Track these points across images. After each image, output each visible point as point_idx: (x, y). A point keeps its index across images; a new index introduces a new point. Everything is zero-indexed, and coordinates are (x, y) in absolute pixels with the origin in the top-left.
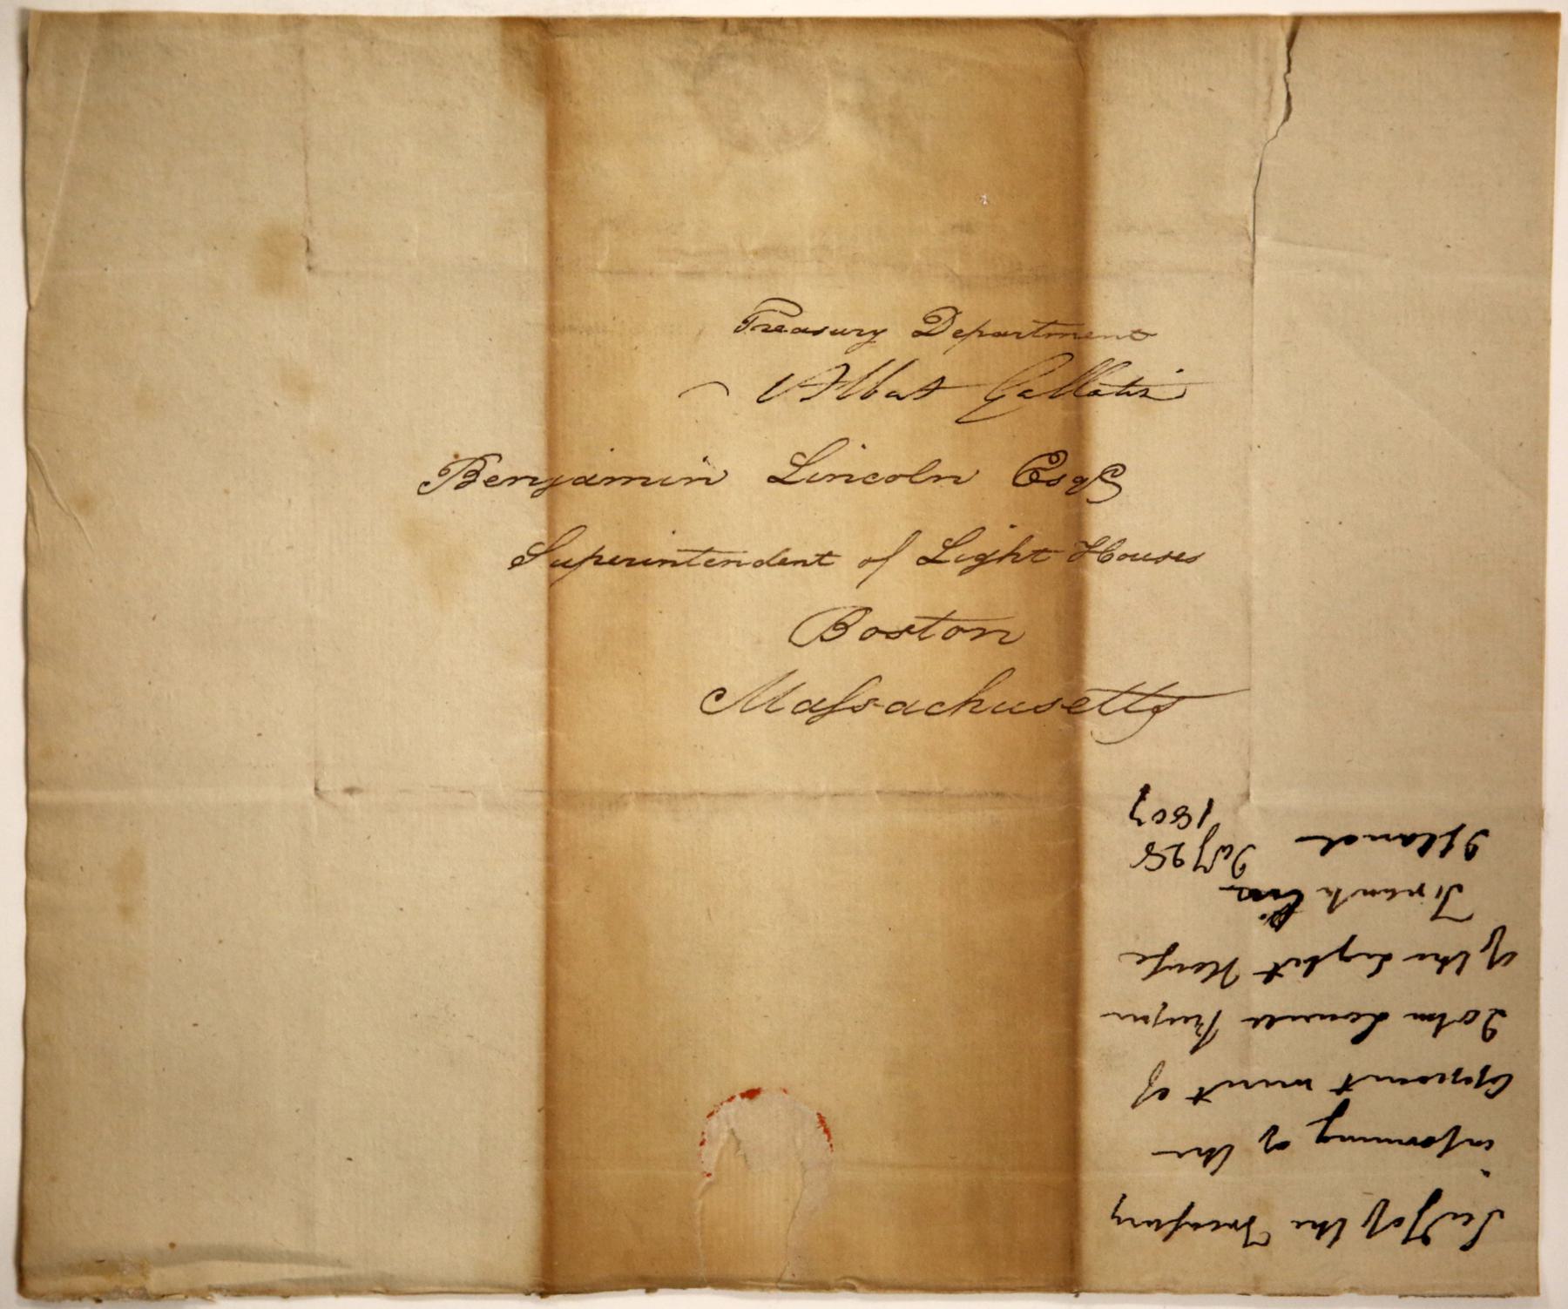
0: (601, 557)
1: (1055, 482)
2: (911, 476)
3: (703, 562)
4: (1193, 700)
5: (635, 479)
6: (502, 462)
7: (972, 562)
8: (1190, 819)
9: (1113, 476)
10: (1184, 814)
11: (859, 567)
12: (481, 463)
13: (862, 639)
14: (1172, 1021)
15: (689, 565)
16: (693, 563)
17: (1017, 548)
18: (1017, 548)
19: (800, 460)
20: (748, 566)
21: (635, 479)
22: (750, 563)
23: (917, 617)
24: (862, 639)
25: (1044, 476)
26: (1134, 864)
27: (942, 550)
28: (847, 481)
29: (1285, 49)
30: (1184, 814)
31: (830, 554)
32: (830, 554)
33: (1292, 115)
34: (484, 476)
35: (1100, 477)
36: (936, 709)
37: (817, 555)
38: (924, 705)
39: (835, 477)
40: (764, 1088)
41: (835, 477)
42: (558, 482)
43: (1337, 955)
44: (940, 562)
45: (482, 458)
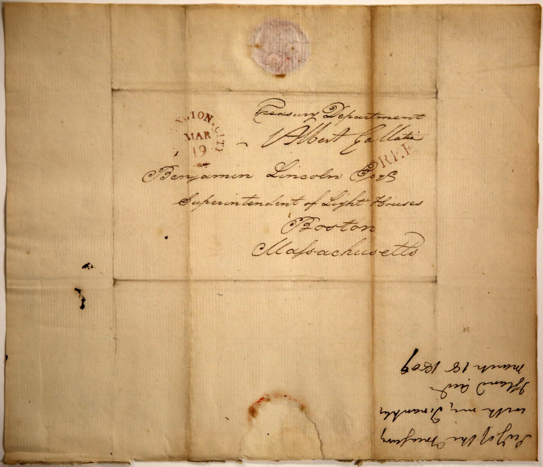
1: (310, 252)
2: (321, 176)
4: (284, 239)
8: (459, 369)
9: (393, 174)
10: (457, 367)
12: (171, 169)
13: (388, 251)
14: (415, 440)
20: (199, 179)
23: (368, 114)
24: (388, 251)
28: (295, 178)
29: (386, 137)
30: (457, 367)
34: (172, 175)
35: (388, 175)
38: (301, 176)
39: (290, 176)
40: (254, 420)
41: (290, 176)
42: (196, 178)
43: (513, 436)
45: (172, 167)
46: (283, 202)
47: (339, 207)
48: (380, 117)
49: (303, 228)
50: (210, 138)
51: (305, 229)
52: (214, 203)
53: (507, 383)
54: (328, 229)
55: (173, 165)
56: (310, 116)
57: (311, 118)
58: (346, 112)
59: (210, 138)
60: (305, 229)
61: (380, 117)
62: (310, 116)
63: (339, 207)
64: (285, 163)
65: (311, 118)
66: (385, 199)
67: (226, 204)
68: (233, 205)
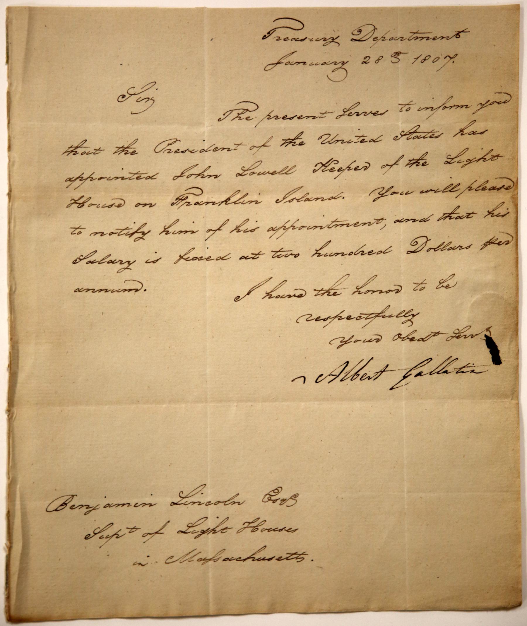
0: (83, 177)
3: (77, 233)
5: (318, 227)
6: (340, 46)
7: (200, 533)
11: (136, 206)
15: (235, 204)
16: (289, 558)
17: (485, 156)
18: (485, 156)
19: (345, 110)
21: (318, 227)
22: (96, 179)
25: (273, 498)
26: (328, 76)
27: (439, 284)
31: (473, 213)
32: (473, 213)
33: (348, 74)
36: (263, 530)
37: (467, 213)
44: (180, 504)
46: (370, 343)
47: (466, 165)
48: (337, 225)
49: (243, 527)
50: (312, 39)
51: (245, 528)
52: (74, 508)
53: (286, 559)
54: (215, 560)
55: (280, 249)
56: (340, 65)
57: (341, 68)
58: (337, 167)
59: (312, 39)
60: (245, 528)
61: (337, 225)
62: (340, 65)
63: (466, 165)
64: (351, 34)
65: (341, 68)
66: (438, 111)
67: (331, 255)
68: (369, 339)
